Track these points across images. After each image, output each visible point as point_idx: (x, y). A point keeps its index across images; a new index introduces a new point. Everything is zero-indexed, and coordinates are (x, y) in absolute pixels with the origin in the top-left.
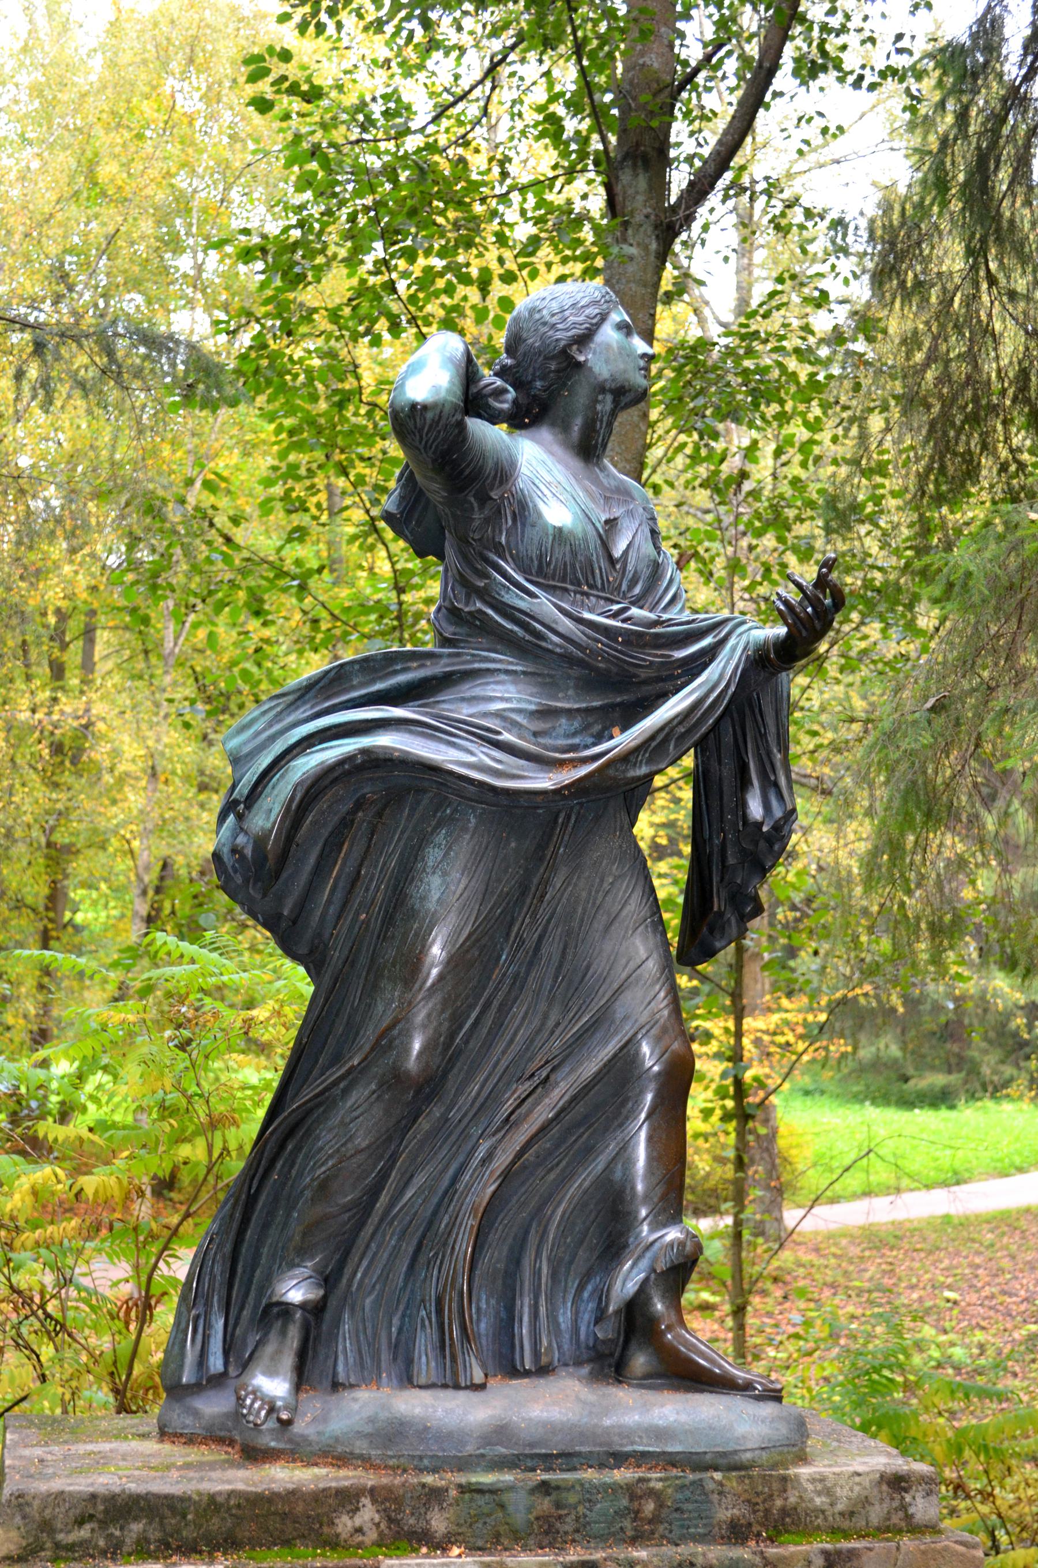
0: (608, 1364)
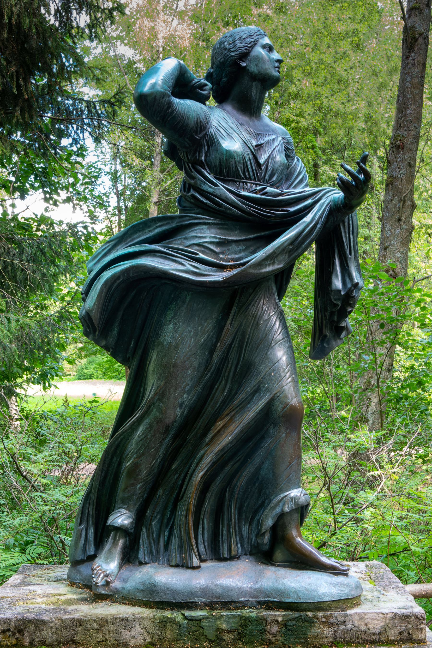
0: (265, 556)
